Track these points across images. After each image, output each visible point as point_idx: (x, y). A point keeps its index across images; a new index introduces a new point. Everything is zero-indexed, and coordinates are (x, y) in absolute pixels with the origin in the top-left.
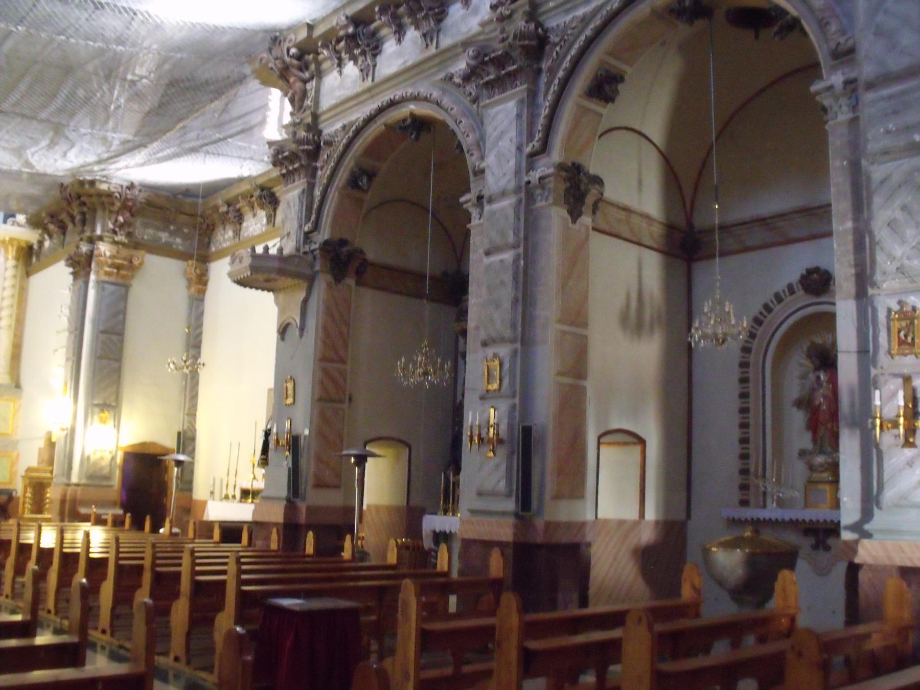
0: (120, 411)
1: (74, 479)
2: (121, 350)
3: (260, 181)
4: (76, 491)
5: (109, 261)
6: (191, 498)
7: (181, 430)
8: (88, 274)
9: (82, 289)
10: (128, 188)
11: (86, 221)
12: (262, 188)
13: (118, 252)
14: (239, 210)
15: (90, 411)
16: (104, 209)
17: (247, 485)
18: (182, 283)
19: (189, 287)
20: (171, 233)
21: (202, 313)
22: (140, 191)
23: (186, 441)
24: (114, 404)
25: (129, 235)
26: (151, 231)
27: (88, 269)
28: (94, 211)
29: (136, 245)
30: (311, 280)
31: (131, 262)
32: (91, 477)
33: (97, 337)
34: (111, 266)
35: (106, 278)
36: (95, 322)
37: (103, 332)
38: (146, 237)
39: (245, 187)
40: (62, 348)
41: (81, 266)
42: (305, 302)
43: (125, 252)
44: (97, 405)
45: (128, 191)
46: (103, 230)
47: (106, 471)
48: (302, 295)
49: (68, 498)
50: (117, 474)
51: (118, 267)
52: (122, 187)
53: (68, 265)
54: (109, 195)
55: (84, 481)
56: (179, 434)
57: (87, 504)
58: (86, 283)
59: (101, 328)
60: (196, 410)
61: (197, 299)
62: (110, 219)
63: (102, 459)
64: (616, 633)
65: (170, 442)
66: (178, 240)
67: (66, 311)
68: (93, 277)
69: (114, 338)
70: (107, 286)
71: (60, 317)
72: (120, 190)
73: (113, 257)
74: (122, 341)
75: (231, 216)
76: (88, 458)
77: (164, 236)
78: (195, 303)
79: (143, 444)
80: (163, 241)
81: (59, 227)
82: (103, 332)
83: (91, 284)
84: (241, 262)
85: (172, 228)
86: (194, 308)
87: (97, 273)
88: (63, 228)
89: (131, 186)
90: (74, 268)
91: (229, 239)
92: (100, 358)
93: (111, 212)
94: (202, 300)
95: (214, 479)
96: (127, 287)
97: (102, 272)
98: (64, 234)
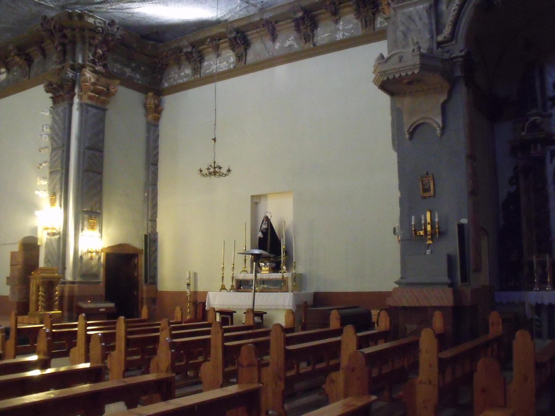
0: (102, 217)
1: (69, 277)
2: (101, 164)
3: (236, 25)
4: (73, 288)
5: (92, 88)
6: (157, 290)
7: (145, 233)
8: (72, 98)
9: (67, 111)
10: (109, 24)
11: (66, 50)
12: (238, 31)
13: (98, 80)
14: (200, 52)
15: (81, 218)
16: (84, 43)
17: (241, 276)
18: (141, 111)
19: (146, 116)
20: (134, 70)
21: (158, 136)
22: (118, 28)
23: (151, 241)
24: (98, 211)
25: (105, 66)
26: (118, 66)
27: (72, 93)
28: (74, 43)
29: (110, 75)
30: (453, 83)
31: (108, 90)
32: (84, 275)
33: (84, 152)
34: (92, 92)
35: (89, 102)
36: (80, 140)
37: (88, 148)
38: (115, 70)
39: (215, 31)
40: (45, 162)
41: (61, 92)
42: (444, 106)
43: (103, 80)
44: (86, 212)
45: (109, 28)
46: (84, 60)
47: (95, 270)
48: (443, 98)
49: (66, 294)
50: (102, 271)
51: (99, 92)
52: (105, 22)
53: (47, 92)
54: (93, 29)
55: (78, 279)
56: (146, 236)
57: (84, 299)
58: (71, 105)
59: (87, 144)
60: (156, 217)
61: (154, 125)
62: (90, 50)
63: (91, 258)
64: (158, 334)
65: (138, 244)
66: (138, 76)
67: (47, 130)
68: (76, 100)
69: (97, 153)
70: (90, 108)
71: (41, 135)
72: (103, 25)
73: (94, 84)
74: (102, 157)
75: (195, 55)
76: (81, 257)
77: (128, 72)
78: (152, 128)
79: (120, 246)
80: (128, 74)
81: (26, 60)
82: (88, 148)
83: (75, 107)
84: (400, 61)
85: (133, 65)
86: (152, 132)
87: (80, 97)
88: (29, 61)
89: (112, 23)
90: (53, 93)
91: (187, 76)
92: (86, 171)
93: (90, 45)
94: (157, 126)
95: (190, 273)
96: (104, 110)
97: (85, 97)
98: (30, 66)
